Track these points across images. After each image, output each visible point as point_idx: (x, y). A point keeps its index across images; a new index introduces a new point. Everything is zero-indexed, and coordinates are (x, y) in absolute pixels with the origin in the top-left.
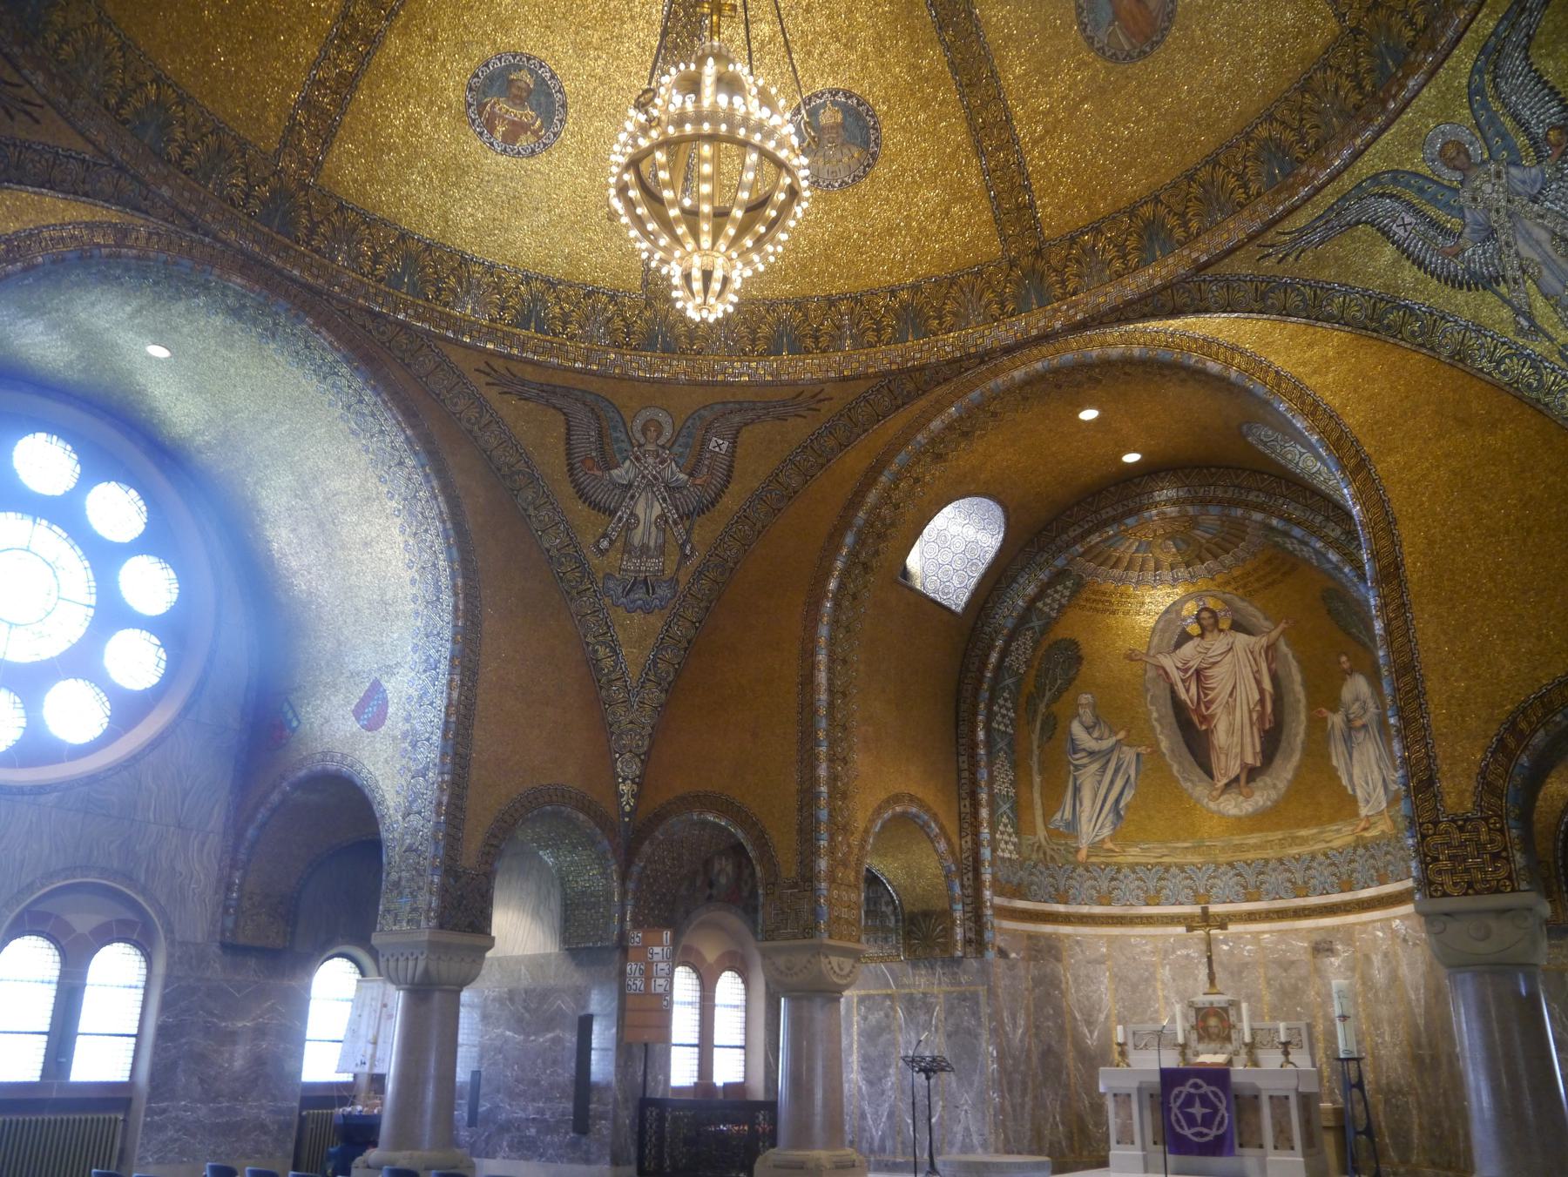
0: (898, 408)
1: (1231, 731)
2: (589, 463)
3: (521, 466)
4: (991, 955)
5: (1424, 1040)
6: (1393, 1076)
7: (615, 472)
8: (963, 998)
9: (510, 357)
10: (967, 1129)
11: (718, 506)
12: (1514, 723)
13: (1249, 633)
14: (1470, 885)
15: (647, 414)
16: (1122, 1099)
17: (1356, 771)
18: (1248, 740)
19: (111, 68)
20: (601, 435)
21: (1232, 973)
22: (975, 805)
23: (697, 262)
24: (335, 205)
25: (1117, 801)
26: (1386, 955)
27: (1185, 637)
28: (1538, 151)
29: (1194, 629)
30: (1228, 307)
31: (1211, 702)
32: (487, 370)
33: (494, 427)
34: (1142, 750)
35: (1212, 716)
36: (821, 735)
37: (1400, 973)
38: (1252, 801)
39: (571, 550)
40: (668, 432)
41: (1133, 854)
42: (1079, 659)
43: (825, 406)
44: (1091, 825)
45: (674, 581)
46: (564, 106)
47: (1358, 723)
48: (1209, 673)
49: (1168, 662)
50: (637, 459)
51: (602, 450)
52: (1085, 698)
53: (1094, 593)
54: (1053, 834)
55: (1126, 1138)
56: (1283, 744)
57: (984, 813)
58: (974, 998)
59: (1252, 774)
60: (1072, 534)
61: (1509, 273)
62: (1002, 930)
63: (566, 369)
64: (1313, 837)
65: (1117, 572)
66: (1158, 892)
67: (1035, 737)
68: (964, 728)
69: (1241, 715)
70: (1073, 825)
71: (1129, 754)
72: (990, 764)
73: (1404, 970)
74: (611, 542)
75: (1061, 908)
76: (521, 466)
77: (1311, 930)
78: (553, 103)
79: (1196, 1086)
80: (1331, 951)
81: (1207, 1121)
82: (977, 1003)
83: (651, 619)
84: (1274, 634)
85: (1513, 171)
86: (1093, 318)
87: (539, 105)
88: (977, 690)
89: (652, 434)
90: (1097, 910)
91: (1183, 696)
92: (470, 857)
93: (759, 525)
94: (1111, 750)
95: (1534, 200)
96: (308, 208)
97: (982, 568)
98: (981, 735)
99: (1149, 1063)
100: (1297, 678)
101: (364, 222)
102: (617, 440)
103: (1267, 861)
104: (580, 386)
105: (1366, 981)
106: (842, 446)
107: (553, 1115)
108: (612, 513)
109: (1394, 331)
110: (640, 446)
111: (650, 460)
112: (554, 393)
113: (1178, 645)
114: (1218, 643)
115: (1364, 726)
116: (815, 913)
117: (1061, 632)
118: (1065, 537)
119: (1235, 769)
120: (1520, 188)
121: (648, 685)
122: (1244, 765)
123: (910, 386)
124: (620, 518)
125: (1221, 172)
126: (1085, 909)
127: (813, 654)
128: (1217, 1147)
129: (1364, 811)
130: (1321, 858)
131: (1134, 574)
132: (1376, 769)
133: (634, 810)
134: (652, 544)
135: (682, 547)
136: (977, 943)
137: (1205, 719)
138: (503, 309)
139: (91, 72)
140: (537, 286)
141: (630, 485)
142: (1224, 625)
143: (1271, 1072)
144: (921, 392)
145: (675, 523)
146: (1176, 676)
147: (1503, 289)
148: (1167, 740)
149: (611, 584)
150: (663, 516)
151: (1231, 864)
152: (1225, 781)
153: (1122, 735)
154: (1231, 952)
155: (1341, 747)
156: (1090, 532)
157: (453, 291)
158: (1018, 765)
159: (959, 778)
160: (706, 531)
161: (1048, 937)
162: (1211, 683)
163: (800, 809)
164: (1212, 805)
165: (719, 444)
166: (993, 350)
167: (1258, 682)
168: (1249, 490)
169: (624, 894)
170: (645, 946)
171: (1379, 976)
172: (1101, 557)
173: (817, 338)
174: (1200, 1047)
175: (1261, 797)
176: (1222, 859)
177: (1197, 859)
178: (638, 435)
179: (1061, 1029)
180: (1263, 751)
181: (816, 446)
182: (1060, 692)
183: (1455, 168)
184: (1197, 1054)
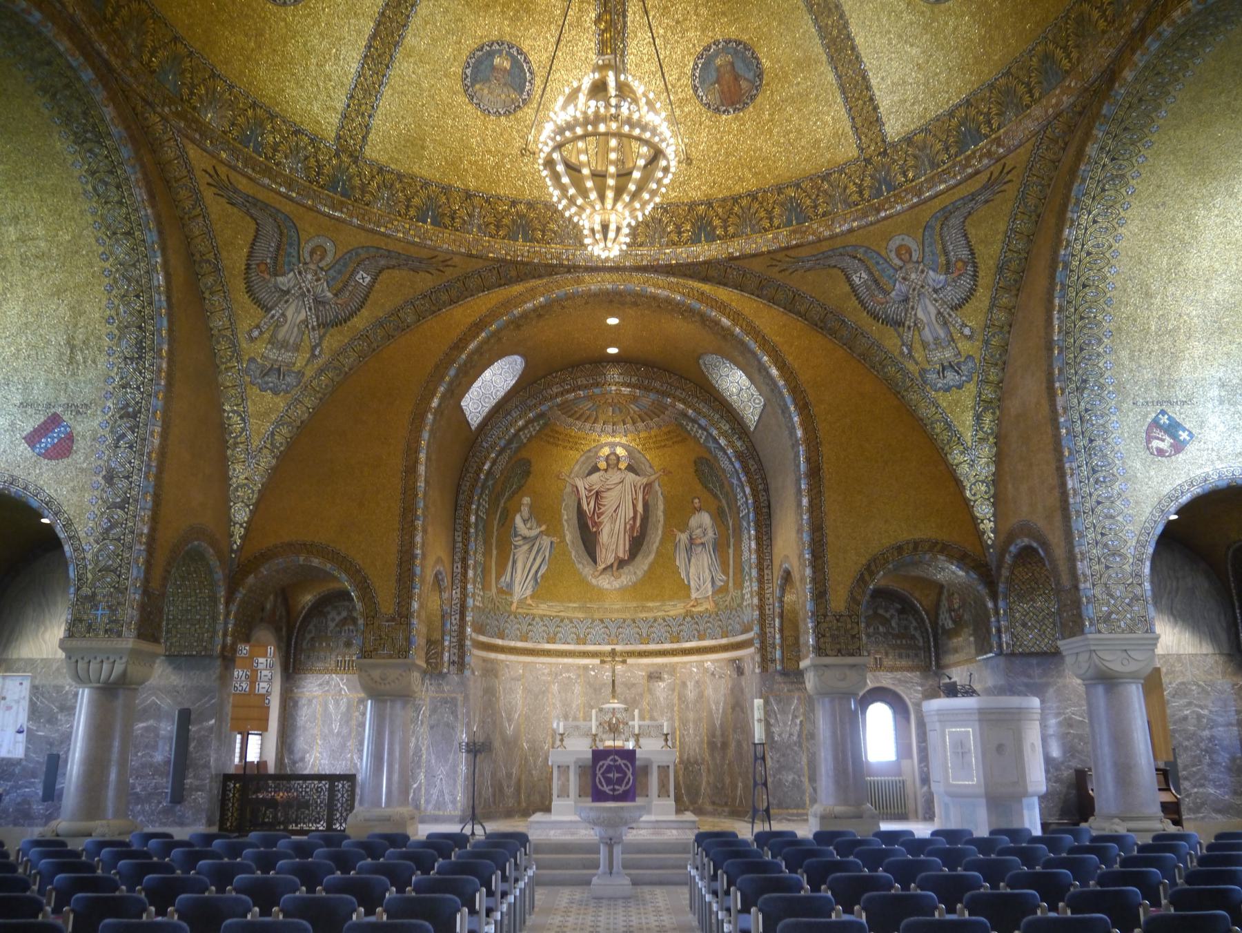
0: (500, 286)
1: (611, 534)
2: (263, 267)
3: (211, 256)
4: (467, 673)
5: (718, 733)
6: (692, 753)
7: (280, 279)
8: (445, 701)
9: (234, 168)
10: (441, 792)
11: (349, 323)
12: (869, 566)
13: (637, 474)
14: (839, 651)
15: (320, 241)
16: (564, 769)
17: (692, 570)
18: (621, 542)
20: (278, 248)
21: (595, 690)
22: (465, 568)
23: (597, 219)
25: (537, 572)
26: (697, 682)
27: (596, 469)
28: (948, 268)
29: (603, 465)
30: (740, 287)
31: (602, 514)
32: (212, 172)
33: (200, 220)
34: (555, 539)
35: (601, 523)
36: (419, 512)
37: (706, 693)
38: (619, 581)
39: (228, 333)
40: (329, 259)
41: (543, 609)
42: (527, 473)
43: (449, 271)
44: (521, 588)
45: (301, 374)
47: (699, 541)
48: (604, 495)
49: (580, 484)
50: (300, 273)
51: (275, 259)
52: (526, 500)
53: (552, 430)
54: (500, 591)
55: (564, 793)
56: (644, 547)
57: (471, 573)
58: (453, 702)
59: (622, 563)
60: (555, 390)
61: (907, 323)
62: (475, 656)
64: (656, 608)
65: (570, 420)
66: (555, 635)
67: (496, 523)
68: (460, 513)
69: (619, 525)
70: (510, 585)
71: (546, 541)
72: (476, 540)
73: (709, 692)
74: (261, 333)
75: (500, 642)
76: (211, 256)
77: (647, 665)
79: (615, 761)
80: (660, 678)
81: (619, 781)
82: (456, 706)
83: (277, 400)
84: (653, 477)
85: (931, 273)
86: (652, 267)
88: (473, 486)
89: (316, 257)
90: (520, 644)
91: (585, 507)
92: (155, 585)
93: (375, 345)
94: (536, 537)
95: (936, 291)
97: (493, 402)
98: (473, 519)
99: (580, 748)
100: (661, 507)
102: (289, 255)
103: (624, 621)
104: (278, 206)
105: (681, 697)
106: (452, 302)
107: (144, 789)
108: (268, 310)
109: (833, 333)
110: (305, 263)
111: (309, 277)
112: (255, 205)
113: (590, 473)
114: (615, 477)
115: (703, 544)
116: (409, 641)
117: (524, 454)
118: (549, 391)
119: (611, 560)
120: (931, 282)
121: (265, 451)
122: (617, 558)
123: (513, 273)
124: (273, 316)
125: (756, 205)
126: (512, 644)
127: (417, 451)
128: (627, 796)
129: (694, 595)
130: (660, 621)
131: (588, 425)
132: (707, 571)
133: (241, 548)
134: (291, 341)
135: (313, 348)
136: (461, 664)
137: (596, 524)
138: (233, 124)
141: (288, 292)
142: (623, 466)
143: (650, 749)
144: (520, 279)
145: (313, 328)
146: (583, 493)
147: (901, 329)
148: (570, 534)
149: (253, 366)
150: (305, 322)
151: (602, 621)
152: (603, 566)
153: (544, 528)
154: (596, 676)
155: (684, 554)
156: (568, 392)
158: (487, 542)
159: (454, 548)
160: (334, 340)
161: (492, 661)
162: (604, 502)
163: (400, 565)
164: (594, 581)
165: (363, 278)
166: (579, 267)
167: (634, 506)
168: (677, 388)
169: (227, 614)
170: (251, 658)
171: (691, 694)
172: (567, 409)
173: (453, 219)
174: (604, 737)
175: (627, 578)
176: (597, 616)
177: (581, 615)
178: (307, 256)
179: (494, 722)
180: (630, 550)
181: (433, 297)
182: (514, 493)
183: (901, 259)
184: (601, 740)
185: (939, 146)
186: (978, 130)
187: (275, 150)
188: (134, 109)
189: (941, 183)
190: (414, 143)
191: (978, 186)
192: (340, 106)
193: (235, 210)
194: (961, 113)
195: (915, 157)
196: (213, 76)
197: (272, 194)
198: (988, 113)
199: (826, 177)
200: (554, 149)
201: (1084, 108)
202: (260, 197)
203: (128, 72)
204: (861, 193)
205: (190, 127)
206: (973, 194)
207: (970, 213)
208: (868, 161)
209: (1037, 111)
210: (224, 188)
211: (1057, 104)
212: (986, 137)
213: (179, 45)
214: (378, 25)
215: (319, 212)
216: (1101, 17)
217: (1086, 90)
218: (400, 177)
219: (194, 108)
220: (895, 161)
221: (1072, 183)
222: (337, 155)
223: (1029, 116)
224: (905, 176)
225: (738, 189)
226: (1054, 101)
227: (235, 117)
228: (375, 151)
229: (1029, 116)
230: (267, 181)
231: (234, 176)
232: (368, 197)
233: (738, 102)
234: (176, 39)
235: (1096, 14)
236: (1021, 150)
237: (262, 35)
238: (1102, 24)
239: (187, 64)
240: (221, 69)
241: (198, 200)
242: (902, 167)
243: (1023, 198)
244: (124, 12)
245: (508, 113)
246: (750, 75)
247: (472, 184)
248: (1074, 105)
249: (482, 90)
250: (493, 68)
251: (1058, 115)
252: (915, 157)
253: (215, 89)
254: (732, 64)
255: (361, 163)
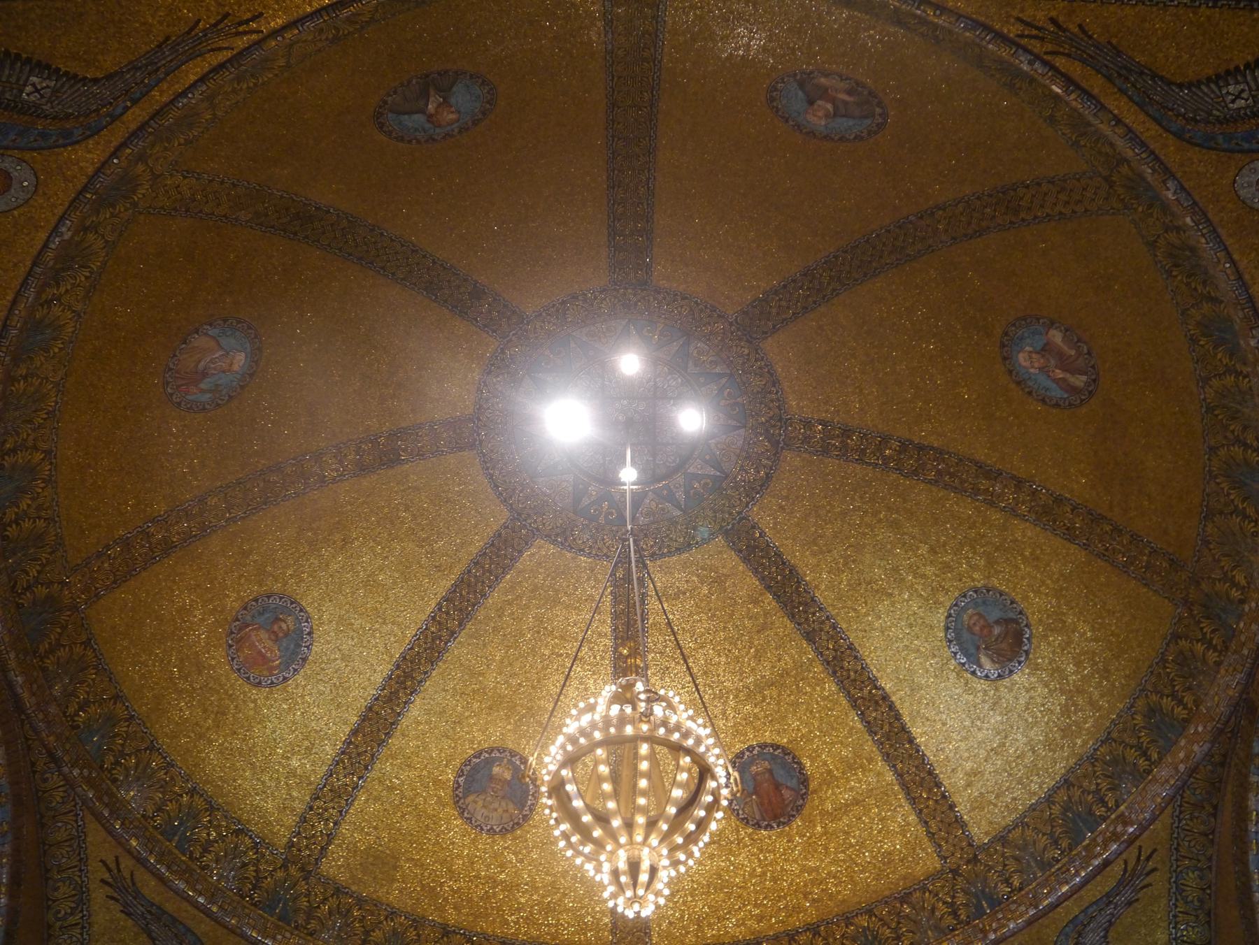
9: (142, 862)
19: (30, 422)
24: (84, 638)
46: (304, 660)
63: (188, 899)
78: (297, 653)
87: (287, 649)
96: (64, 628)
101: (96, 667)
138: (159, 810)
139: (17, 413)
140: (199, 803)
157: (127, 769)
185: (1044, 841)
186: (1090, 813)
187: (206, 850)
188: (33, 764)
189: (1061, 884)
190: (382, 862)
191: (1112, 883)
192: (299, 807)
193: (130, 922)
194: (1062, 796)
195: (1016, 859)
196: (151, 748)
197: (185, 905)
198: (1098, 791)
199: (905, 898)
200: (563, 765)
201: (1225, 756)
202: (169, 907)
203: (41, 716)
204: (955, 914)
205: (100, 799)
206: (1108, 895)
207: (1111, 923)
208: (956, 872)
209: (1163, 772)
210: (123, 891)
211: (1187, 757)
212: (1104, 819)
213: (119, 705)
214: (363, 720)
215: (243, 936)
216: (1208, 649)
217: (1221, 731)
218: (360, 902)
219: (115, 781)
220: (991, 868)
221: (1246, 853)
222: (284, 866)
223: (1155, 780)
224: (1009, 884)
225: (796, 921)
226: (1182, 755)
227: (164, 802)
228: (335, 865)
229: (1155, 780)
230: (182, 886)
231: (142, 876)
232: (313, 925)
233: (782, 815)
234: (117, 698)
235: (1199, 648)
236: (1158, 825)
237: (224, 714)
238: (1212, 656)
239: (122, 728)
240: (164, 742)
241: (81, 898)
242: (1001, 874)
243: (1180, 891)
244: (62, 653)
245: (504, 832)
246: (793, 783)
247: (452, 916)
248: (1209, 755)
249: (476, 804)
250: (491, 778)
251: (1193, 771)
252: (1016, 859)
253: (148, 764)
254: (770, 771)
255: (312, 880)
